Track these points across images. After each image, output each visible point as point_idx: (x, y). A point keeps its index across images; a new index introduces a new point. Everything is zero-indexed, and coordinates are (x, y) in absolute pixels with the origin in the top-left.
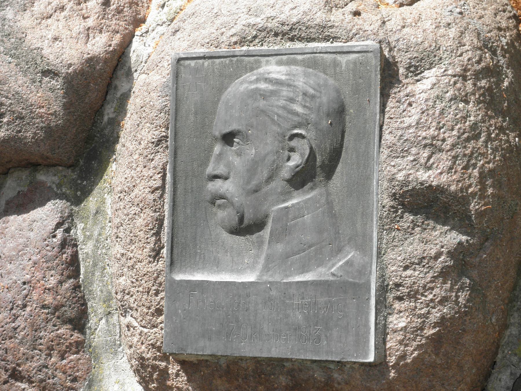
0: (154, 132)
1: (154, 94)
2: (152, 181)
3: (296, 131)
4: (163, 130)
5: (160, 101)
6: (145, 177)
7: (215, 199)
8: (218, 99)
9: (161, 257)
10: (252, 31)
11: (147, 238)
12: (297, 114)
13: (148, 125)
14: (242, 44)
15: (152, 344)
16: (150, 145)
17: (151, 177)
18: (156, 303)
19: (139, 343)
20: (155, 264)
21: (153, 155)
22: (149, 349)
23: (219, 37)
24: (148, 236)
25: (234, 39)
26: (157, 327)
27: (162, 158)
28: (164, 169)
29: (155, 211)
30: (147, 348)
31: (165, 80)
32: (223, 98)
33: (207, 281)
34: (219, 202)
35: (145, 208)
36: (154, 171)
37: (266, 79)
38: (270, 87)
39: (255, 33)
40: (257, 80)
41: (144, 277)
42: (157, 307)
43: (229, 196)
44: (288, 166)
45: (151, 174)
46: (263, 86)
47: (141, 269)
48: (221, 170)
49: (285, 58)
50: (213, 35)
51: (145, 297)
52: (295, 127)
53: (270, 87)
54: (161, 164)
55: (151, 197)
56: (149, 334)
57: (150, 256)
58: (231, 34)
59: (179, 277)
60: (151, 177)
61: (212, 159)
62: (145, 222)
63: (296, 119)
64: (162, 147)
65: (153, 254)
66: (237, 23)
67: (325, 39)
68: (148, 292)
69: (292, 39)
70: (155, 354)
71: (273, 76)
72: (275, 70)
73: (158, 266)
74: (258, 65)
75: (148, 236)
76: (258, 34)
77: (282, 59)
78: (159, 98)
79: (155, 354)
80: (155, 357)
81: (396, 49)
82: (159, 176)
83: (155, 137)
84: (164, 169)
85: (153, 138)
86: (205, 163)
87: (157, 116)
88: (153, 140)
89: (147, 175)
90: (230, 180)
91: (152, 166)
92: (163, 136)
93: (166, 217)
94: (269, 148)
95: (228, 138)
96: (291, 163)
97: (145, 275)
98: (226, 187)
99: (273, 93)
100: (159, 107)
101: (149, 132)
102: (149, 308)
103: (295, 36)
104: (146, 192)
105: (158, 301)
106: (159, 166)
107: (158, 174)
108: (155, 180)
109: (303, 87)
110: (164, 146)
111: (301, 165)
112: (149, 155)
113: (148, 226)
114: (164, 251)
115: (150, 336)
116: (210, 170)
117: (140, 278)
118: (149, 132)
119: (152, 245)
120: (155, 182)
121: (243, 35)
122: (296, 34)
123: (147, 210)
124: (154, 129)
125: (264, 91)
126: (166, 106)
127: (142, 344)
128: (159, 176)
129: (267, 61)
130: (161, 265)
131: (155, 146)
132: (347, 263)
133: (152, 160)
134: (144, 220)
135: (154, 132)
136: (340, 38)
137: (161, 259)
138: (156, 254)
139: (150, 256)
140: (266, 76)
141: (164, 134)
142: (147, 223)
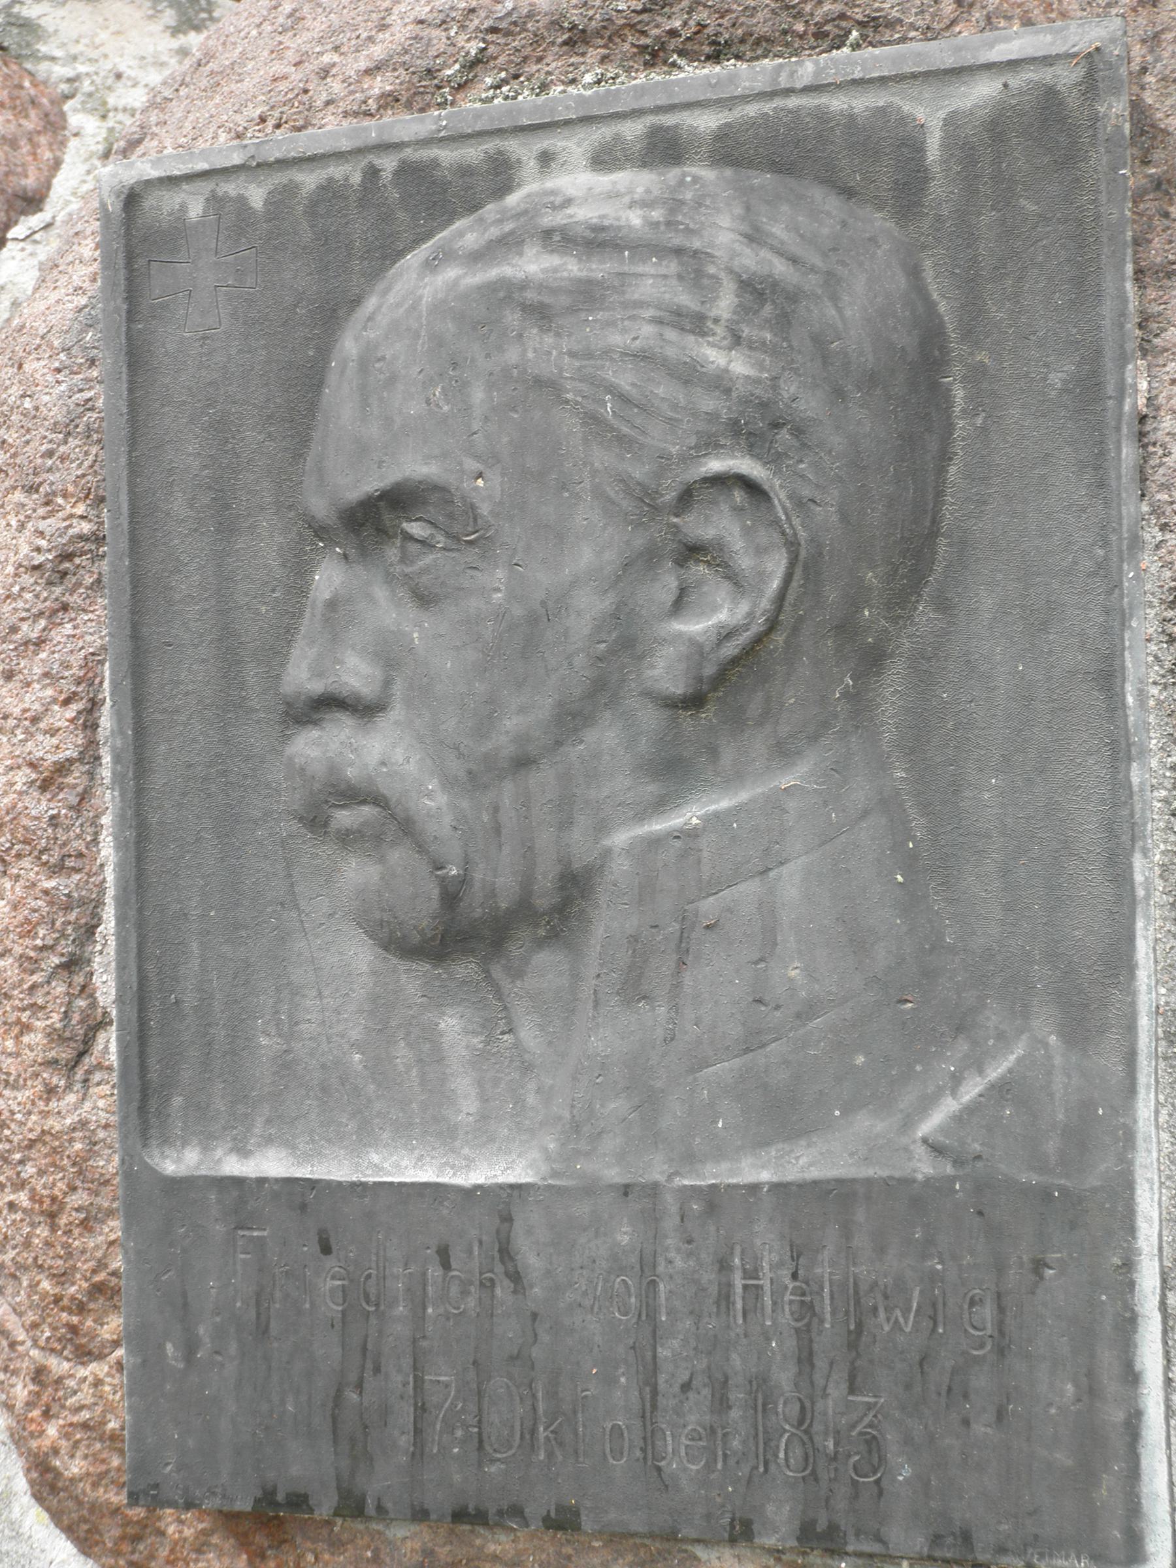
0: (42, 525)
1: (36, 365)
2: (40, 737)
3: (715, 465)
4: (80, 509)
5: (63, 387)
6: (12, 722)
7: (328, 804)
8: (319, 349)
9: (99, 1066)
10: (461, 40)
11: (33, 987)
12: (720, 383)
13: (18, 496)
14: (418, 103)
15: (85, 1426)
16: (27, 579)
17: (35, 720)
18: (92, 1264)
19: (36, 1413)
20: (71, 1098)
21: (43, 623)
22: (77, 1442)
23: (311, 86)
24: (37, 978)
25: (379, 85)
26: (101, 1357)
27: (90, 629)
28: (89, 679)
29: (58, 869)
30: (67, 1436)
31: (83, 301)
32: (349, 345)
33: (312, 1184)
34: (344, 818)
35: (19, 856)
36: (49, 692)
37: (548, 233)
38: (572, 267)
39: (473, 48)
40: (508, 244)
41: (33, 1153)
42: (97, 1278)
43: (385, 787)
44: (680, 634)
45: (37, 706)
46: (533, 264)
47: (18, 1116)
48: (356, 674)
49: (632, 130)
50: (283, 86)
51: (43, 1232)
52: (709, 445)
53: (572, 267)
54: (76, 660)
55: (40, 807)
56: (72, 1383)
57: (52, 1063)
58: (363, 64)
59: (179, 1162)
60: (35, 720)
61: (309, 623)
62: (20, 918)
63: (709, 403)
64: (78, 584)
65: (65, 1054)
66: (388, 21)
67: (820, 35)
68: (52, 1216)
69: (654, 56)
70: (103, 1461)
71: (583, 214)
72: (582, 188)
73: (87, 1105)
74: (501, 176)
75: (37, 978)
76: (492, 49)
77: (617, 138)
78: (60, 377)
79: (103, 1461)
80: (102, 1475)
81: (1150, 79)
82: (71, 711)
83: (43, 543)
84: (89, 679)
85: (38, 550)
86: (277, 650)
87: (50, 454)
88: (39, 559)
89: (17, 711)
90: (397, 712)
91: (38, 670)
92: (81, 537)
93: (109, 899)
94: (585, 557)
95: (372, 522)
96: (696, 627)
97: (32, 1144)
98: (378, 751)
99: (588, 294)
100: (57, 414)
101: (22, 526)
102: (62, 1278)
103: (673, 33)
104: (18, 787)
105: (99, 1254)
106: (68, 667)
107: (66, 702)
108: (53, 732)
109: (734, 255)
110: (88, 580)
111: (746, 627)
112: (25, 627)
113: (30, 933)
114: (109, 1044)
115: (75, 1393)
116: (301, 676)
117: (18, 1156)
118: (22, 526)
119: (56, 1017)
120: (55, 741)
121: (423, 63)
122: (677, 24)
123: (26, 863)
124: (41, 511)
125: (542, 287)
126: (88, 405)
127: (47, 1414)
128: (71, 711)
129: (546, 159)
130: (100, 1103)
131: (50, 583)
132: (1000, 1090)
133: (40, 643)
134: (15, 907)
135: (42, 525)
136: (891, 24)
137: (97, 1077)
138: (75, 1050)
139: (52, 1063)
140: (549, 220)
141: (86, 527)
142: (27, 921)
